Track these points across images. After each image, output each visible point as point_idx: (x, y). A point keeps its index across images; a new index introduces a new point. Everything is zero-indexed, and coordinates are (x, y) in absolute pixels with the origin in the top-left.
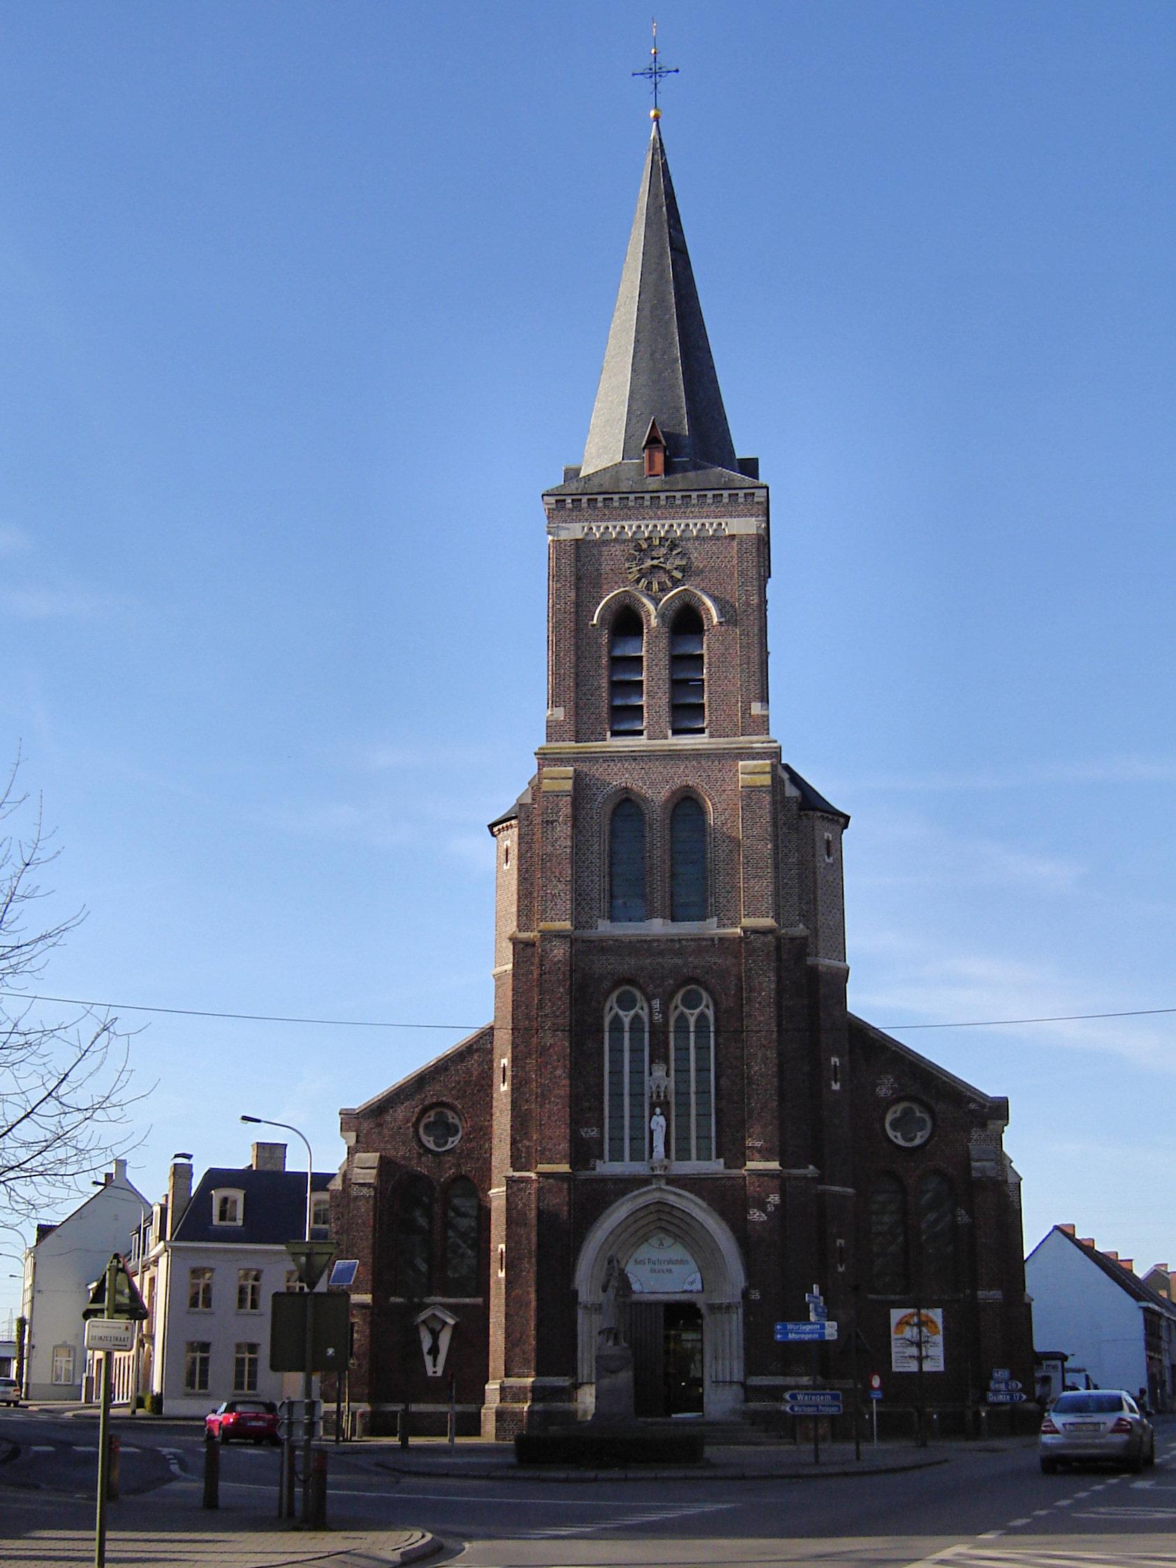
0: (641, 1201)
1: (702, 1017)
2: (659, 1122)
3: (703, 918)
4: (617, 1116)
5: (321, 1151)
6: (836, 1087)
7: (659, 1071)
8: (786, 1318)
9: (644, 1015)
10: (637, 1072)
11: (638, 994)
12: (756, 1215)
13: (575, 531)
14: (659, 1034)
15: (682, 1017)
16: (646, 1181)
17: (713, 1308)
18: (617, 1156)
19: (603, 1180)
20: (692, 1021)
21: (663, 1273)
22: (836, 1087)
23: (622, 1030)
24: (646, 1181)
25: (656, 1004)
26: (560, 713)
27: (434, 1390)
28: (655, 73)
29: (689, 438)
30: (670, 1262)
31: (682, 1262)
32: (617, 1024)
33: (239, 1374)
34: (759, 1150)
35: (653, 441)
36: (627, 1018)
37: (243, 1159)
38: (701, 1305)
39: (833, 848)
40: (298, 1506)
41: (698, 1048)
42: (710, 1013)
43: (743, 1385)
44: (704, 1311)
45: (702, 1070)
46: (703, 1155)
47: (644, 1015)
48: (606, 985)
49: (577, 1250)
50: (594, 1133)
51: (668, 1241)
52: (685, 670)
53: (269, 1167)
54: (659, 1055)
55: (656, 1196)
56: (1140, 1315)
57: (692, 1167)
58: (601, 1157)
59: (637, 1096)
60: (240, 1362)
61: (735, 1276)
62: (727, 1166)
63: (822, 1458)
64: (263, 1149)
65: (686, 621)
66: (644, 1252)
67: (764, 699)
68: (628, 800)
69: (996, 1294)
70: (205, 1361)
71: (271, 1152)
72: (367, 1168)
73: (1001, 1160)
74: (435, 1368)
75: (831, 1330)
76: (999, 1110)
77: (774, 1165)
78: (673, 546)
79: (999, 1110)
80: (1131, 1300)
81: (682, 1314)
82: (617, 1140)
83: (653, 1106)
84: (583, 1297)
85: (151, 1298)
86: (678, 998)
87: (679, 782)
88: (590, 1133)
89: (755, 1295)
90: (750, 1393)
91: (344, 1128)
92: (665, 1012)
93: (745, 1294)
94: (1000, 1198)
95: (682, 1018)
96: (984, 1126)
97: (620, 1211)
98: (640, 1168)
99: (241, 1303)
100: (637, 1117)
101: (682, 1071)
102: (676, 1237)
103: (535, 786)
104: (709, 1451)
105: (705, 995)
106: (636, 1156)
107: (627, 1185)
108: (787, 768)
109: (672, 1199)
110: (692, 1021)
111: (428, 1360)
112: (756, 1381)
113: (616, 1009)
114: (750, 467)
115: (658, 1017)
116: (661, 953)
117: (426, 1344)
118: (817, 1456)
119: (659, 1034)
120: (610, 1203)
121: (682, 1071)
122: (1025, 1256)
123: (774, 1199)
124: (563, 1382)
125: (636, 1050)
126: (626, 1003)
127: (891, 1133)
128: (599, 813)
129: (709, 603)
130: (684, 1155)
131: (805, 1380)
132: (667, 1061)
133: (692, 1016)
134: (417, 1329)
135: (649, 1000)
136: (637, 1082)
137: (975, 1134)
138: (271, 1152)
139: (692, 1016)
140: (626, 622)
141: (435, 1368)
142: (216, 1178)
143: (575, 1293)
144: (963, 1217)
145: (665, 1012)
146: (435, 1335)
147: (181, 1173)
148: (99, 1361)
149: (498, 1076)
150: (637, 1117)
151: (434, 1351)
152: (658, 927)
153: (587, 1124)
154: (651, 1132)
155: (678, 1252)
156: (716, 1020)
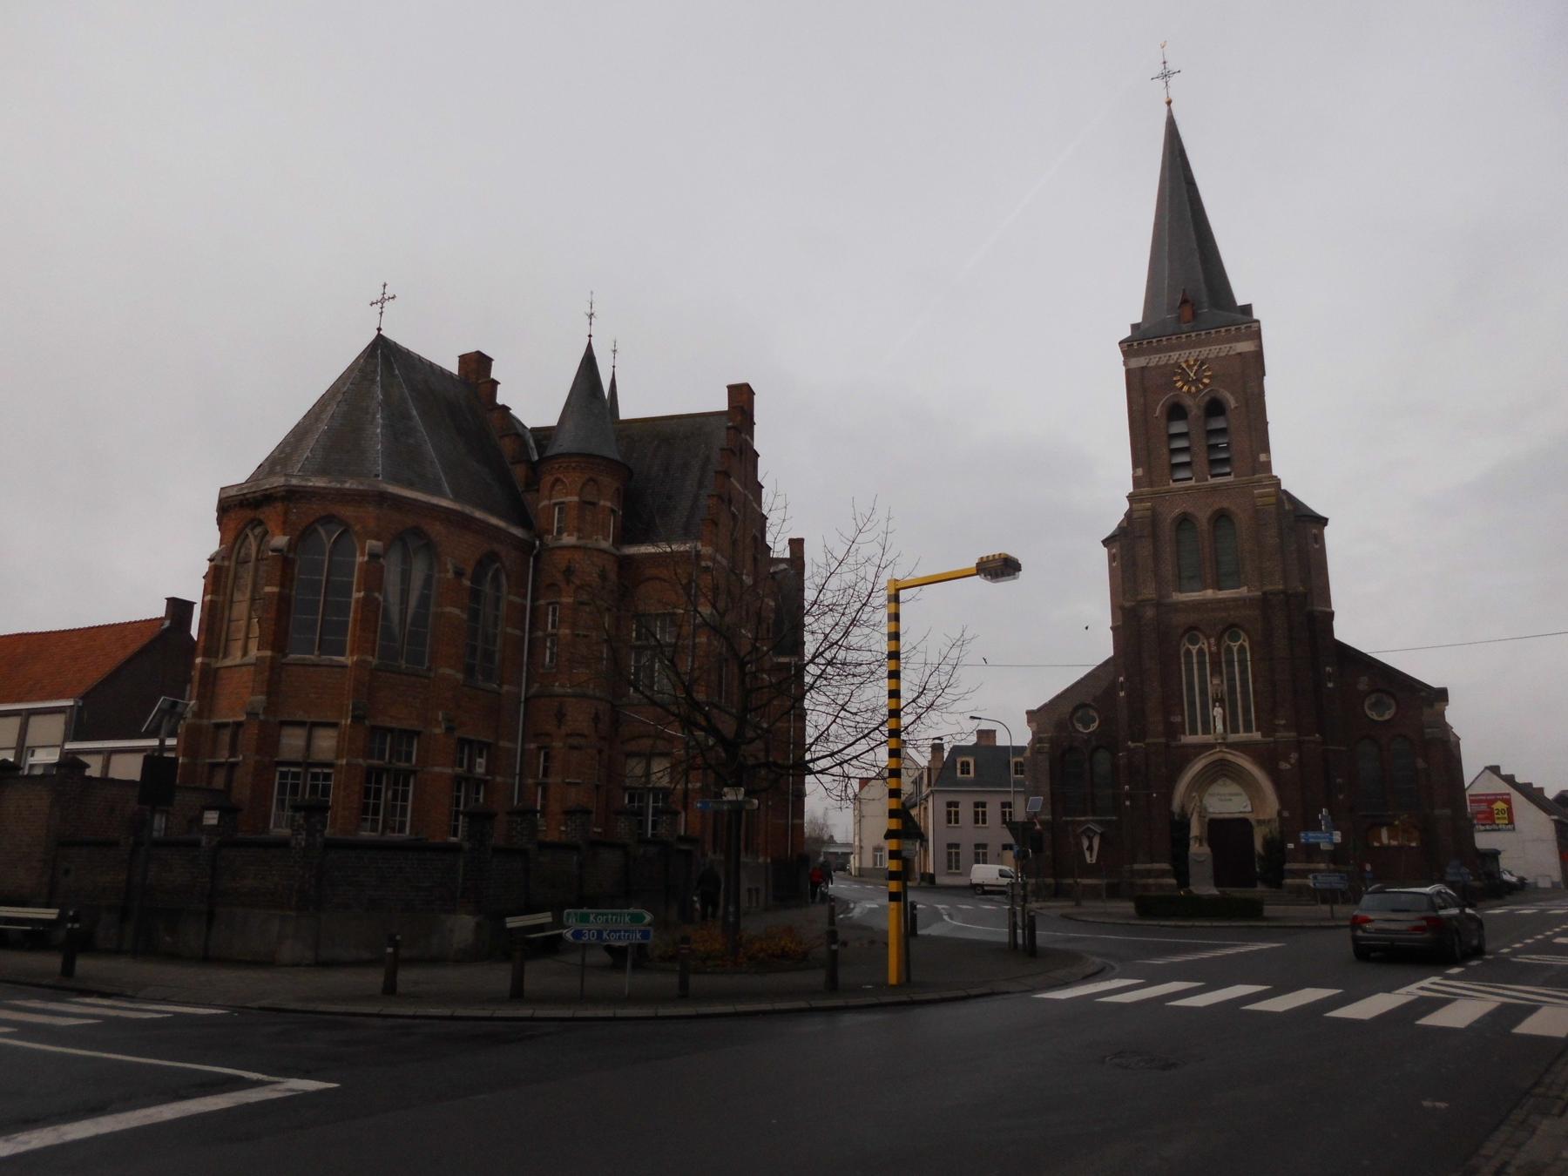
2: (1218, 711)
5: (1017, 734)
6: (1330, 685)
8: (1306, 829)
9: (1205, 647)
12: (1284, 766)
13: (1141, 362)
17: (1260, 822)
18: (1194, 731)
22: (1330, 685)
24: (1213, 746)
25: (1212, 641)
26: (1140, 472)
27: (1089, 871)
32: (1188, 652)
33: (950, 861)
34: (1284, 726)
35: (1184, 301)
36: (1194, 649)
37: (972, 740)
38: (1251, 817)
39: (1319, 539)
40: (1020, 941)
42: (1247, 644)
46: (1248, 729)
47: (1205, 647)
51: (1229, 782)
53: (984, 743)
56: (1552, 826)
57: (1242, 736)
59: (1204, 692)
60: (950, 854)
63: (844, 976)
64: (982, 734)
65: (1215, 408)
69: (1447, 812)
70: (957, 854)
71: (986, 735)
72: (1036, 738)
73: (1446, 728)
74: (1091, 859)
75: (1337, 837)
76: (1441, 695)
77: (1293, 734)
78: (1202, 364)
79: (1441, 695)
80: (1544, 815)
83: (1214, 701)
85: (926, 823)
87: (1216, 507)
89: (1286, 814)
91: (1029, 722)
93: (1279, 814)
94: (1446, 750)
96: (1431, 706)
97: (1197, 766)
98: (1209, 738)
99: (977, 821)
100: (1205, 706)
101: (1231, 679)
102: (1233, 779)
103: (1128, 515)
104: (1268, 910)
106: (1206, 731)
108: (1285, 492)
109: (1229, 757)
111: (1087, 854)
114: (1247, 309)
115: (1214, 649)
117: (1086, 844)
122: (809, 741)
126: (1194, 641)
127: (1368, 712)
130: (1235, 730)
131: (1322, 866)
132: (1221, 673)
138: (986, 735)
141: (1091, 859)
142: (957, 750)
144: (1420, 763)
145: (1218, 644)
146: (1091, 840)
147: (937, 749)
150: (1205, 706)
151: (1090, 848)
155: (1234, 788)
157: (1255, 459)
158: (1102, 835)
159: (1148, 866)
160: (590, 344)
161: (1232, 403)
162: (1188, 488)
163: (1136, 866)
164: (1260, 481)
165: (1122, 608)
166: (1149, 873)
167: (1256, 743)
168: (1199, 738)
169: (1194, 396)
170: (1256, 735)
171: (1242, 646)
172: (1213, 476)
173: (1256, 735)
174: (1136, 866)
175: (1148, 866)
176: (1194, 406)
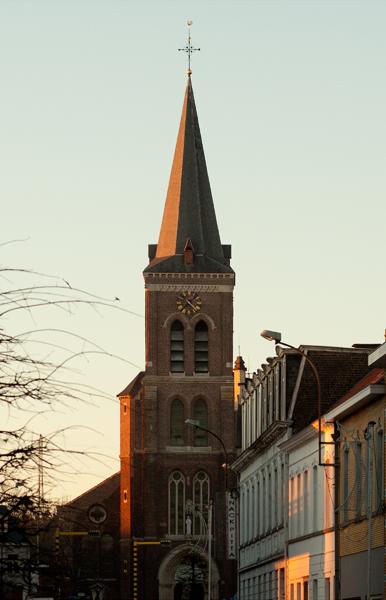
9: (183, 482)
10: (180, 500)
14: (189, 489)
15: (198, 482)
16: (184, 542)
24: (184, 542)
25: (188, 478)
28: (189, 50)
36: (177, 483)
42: (208, 482)
47: (183, 482)
50: (164, 524)
52: (270, 594)
54: (189, 497)
58: (167, 533)
81: (328, 579)
82: (173, 526)
83: (187, 515)
86: (197, 475)
87: (197, 394)
89: (223, 582)
92: (191, 482)
93: (219, 582)
95: (198, 484)
106: (180, 533)
107: (176, 543)
115: (188, 483)
116: (191, 459)
118: (324, 465)
119: (189, 489)
126: (176, 477)
128: (166, 406)
129: (211, 321)
130: (197, 533)
133: (201, 482)
135: (186, 476)
136: (181, 508)
139: (201, 482)
143: (158, 581)
145: (191, 482)
148: (299, 584)
149: (122, 497)
152: (189, 448)
153: (162, 521)
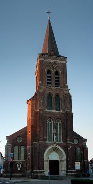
0: (53, 147)
1: (51, 123)
2: (55, 136)
3: (60, 111)
4: (49, 136)
7: (55, 130)
10: (51, 130)
11: (51, 120)
18: (49, 141)
19: (47, 144)
20: (58, 124)
21: (54, 156)
23: (58, 125)
24: (56, 144)
25: (54, 121)
27: (19, 172)
29: (51, 48)
30: (55, 155)
31: (56, 155)
32: (49, 123)
36: (50, 123)
38: (59, 160)
41: (59, 127)
42: (61, 123)
43: (66, 171)
44: (60, 161)
45: (60, 130)
48: (47, 118)
49: (44, 153)
51: (55, 152)
55: (54, 146)
59: (51, 133)
61: (65, 157)
62: (64, 142)
65: (57, 73)
66: (52, 154)
67: (67, 84)
68: (57, 95)
69: (86, 161)
74: (19, 169)
76: (86, 140)
79: (86, 140)
82: (49, 139)
84: (45, 159)
87: (56, 93)
88: (45, 137)
90: (67, 172)
91: (7, 138)
98: (52, 142)
100: (51, 136)
101: (57, 130)
105: (60, 120)
106: (51, 141)
110: (58, 124)
111: (18, 168)
112: (69, 170)
113: (57, 122)
117: (18, 166)
120: (48, 147)
121: (57, 130)
123: (71, 147)
124: (43, 171)
125: (51, 127)
126: (50, 121)
130: (57, 141)
133: (50, 123)
134: (17, 164)
135: (53, 120)
137: (83, 142)
140: (49, 72)
141: (19, 169)
145: (55, 122)
146: (19, 165)
151: (19, 167)
154: (54, 138)
155: (56, 154)
156: (62, 123)
157: (64, 85)
158: (22, 164)
159: (37, 171)
160: (49, 21)
161: (61, 73)
162: (52, 89)
163: (34, 171)
164: (66, 89)
165: (36, 113)
166: (38, 172)
167: (62, 144)
168: (50, 142)
169: (53, 69)
170: (62, 142)
171: (60, 123)
172: (56, 87)
173: (62, 142)
174: (34, 171)
175: (37, 171)
176: (53, 72)
